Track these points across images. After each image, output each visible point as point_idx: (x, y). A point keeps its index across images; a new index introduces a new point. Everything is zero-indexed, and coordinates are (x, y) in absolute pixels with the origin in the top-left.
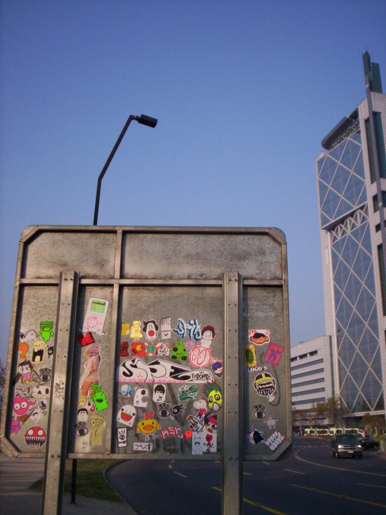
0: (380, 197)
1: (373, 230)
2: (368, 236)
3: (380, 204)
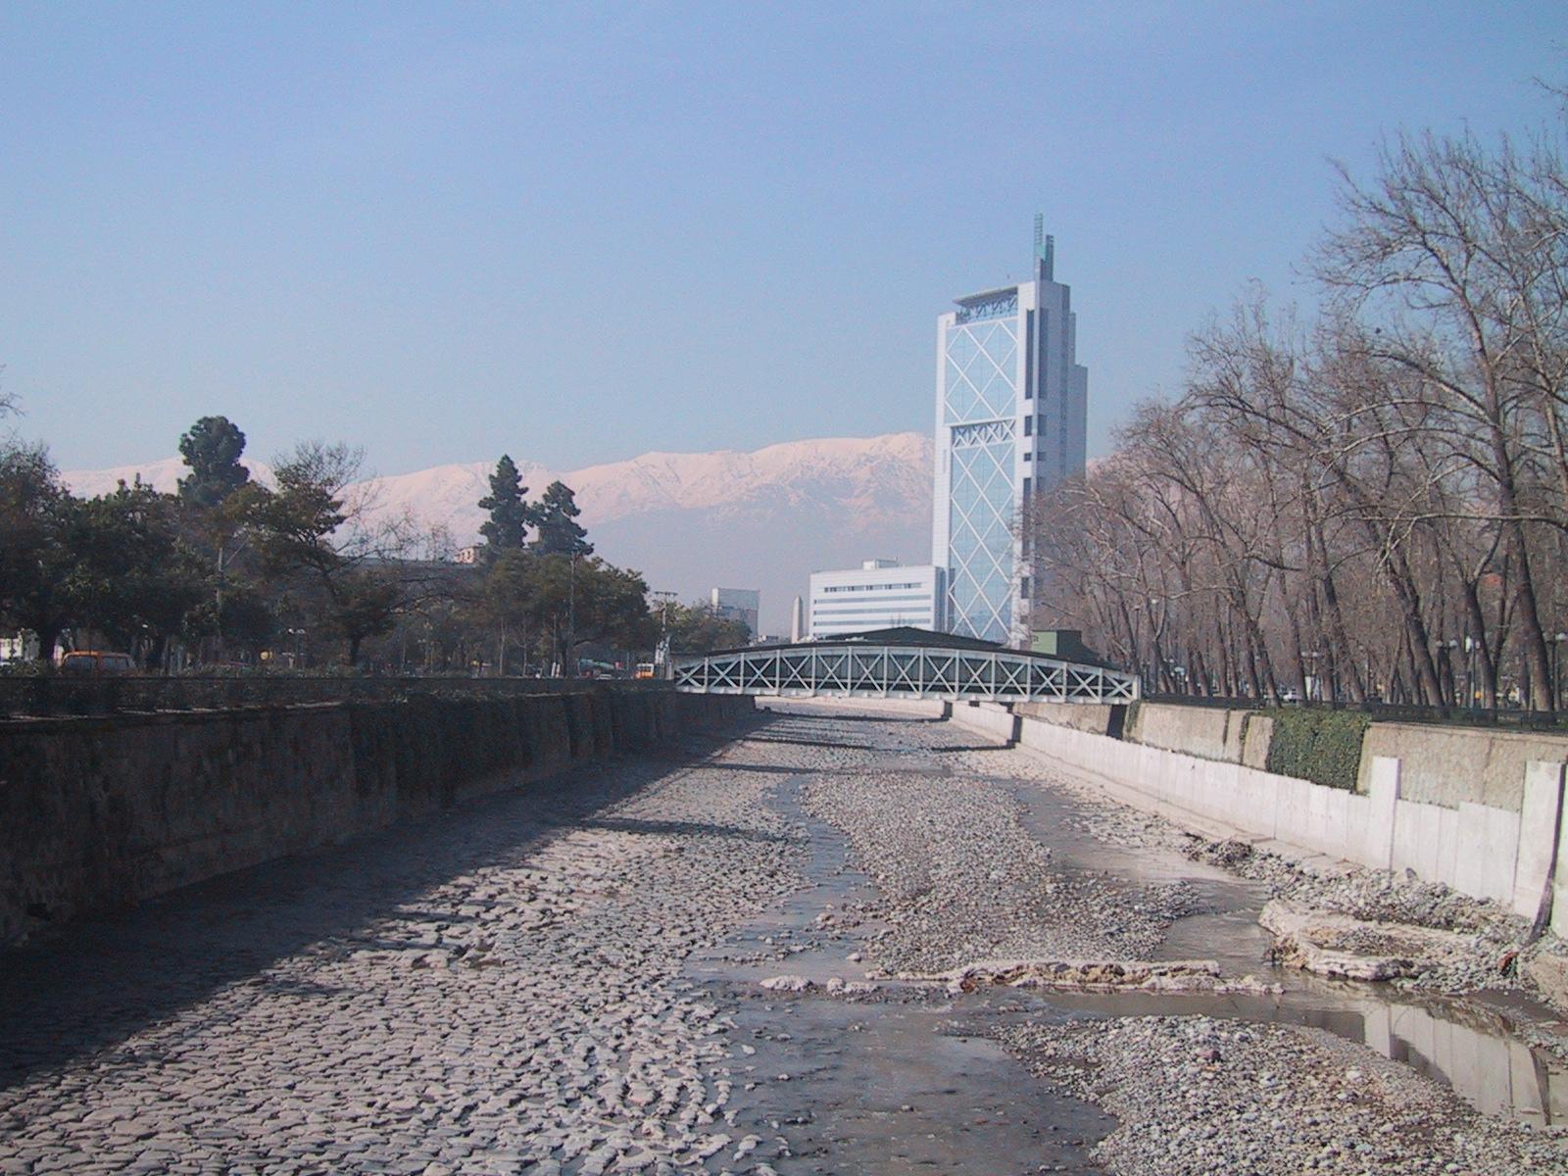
0: (1031, 582)
1: (1019, 457)
2: (1011, 459)
3: (1034, 431)
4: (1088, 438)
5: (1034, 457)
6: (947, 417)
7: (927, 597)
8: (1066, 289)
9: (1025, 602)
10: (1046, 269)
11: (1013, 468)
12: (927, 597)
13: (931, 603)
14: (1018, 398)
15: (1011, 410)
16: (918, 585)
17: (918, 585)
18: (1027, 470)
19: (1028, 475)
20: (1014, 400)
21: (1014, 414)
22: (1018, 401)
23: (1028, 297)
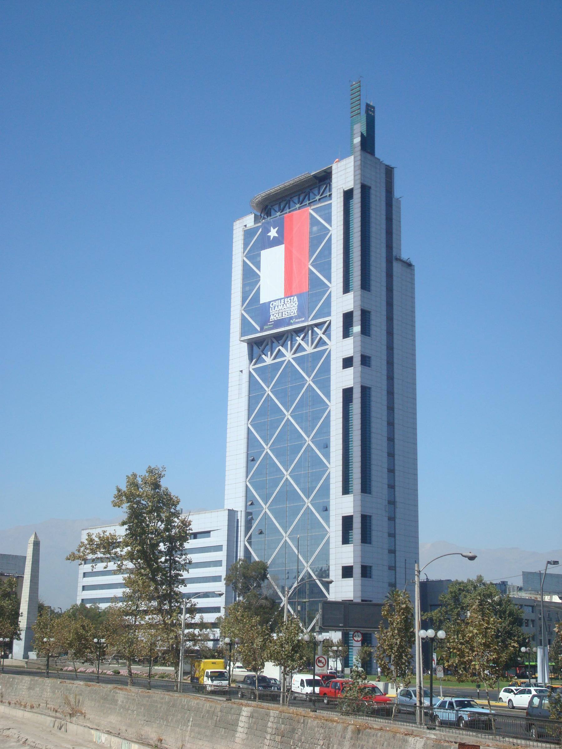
0: (357, 318)
1: (335, 530)
2: (326, 368)
3: (357, 329)
4: (417, 378)
5: (357, 571)
6: (246, 327)
7: (218, 548)
8: (389, 172)
9: (349, 548)
10: (368, 144)
11: (329, 380)
12: (218, 548)
13: (222, 556)
14: (332, 541)
15: (326, 310)
16: (207, 533)
17: (207, 533)
18: (343, 378)
19: (349, 383)
20: (328, 542)
21: (329, 314)
22: (332, 545)
23: (345, 174)
